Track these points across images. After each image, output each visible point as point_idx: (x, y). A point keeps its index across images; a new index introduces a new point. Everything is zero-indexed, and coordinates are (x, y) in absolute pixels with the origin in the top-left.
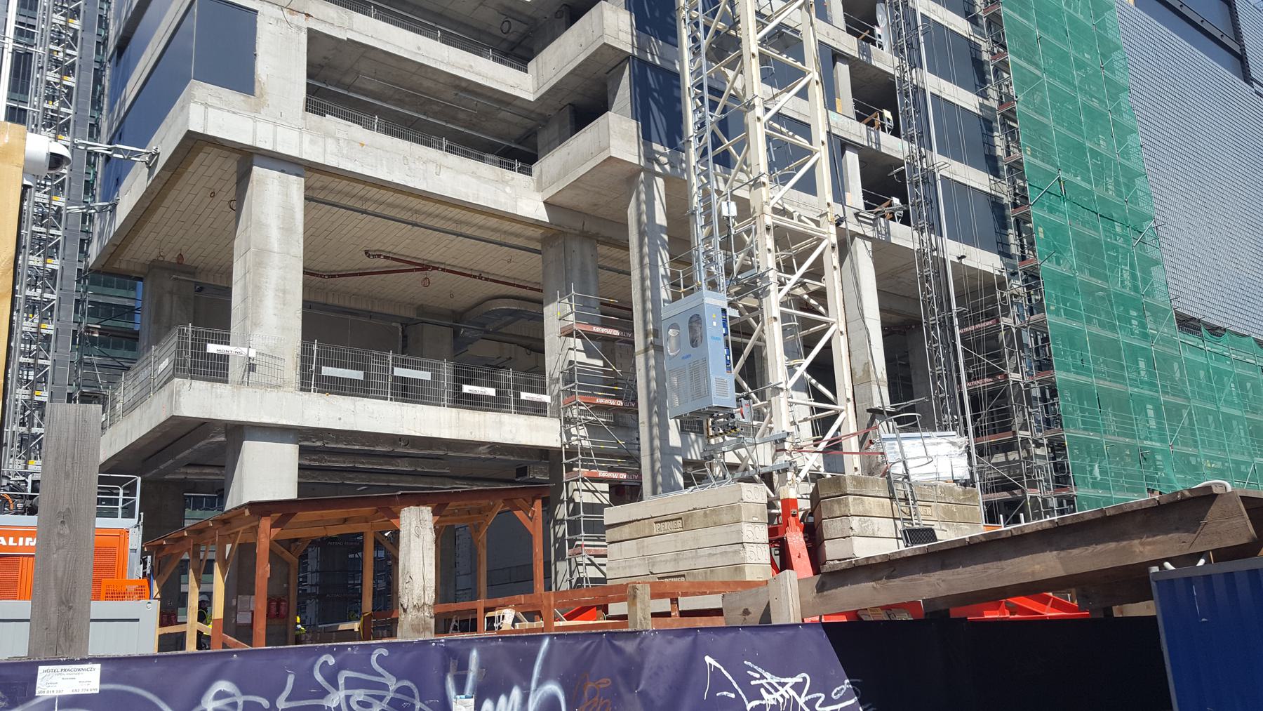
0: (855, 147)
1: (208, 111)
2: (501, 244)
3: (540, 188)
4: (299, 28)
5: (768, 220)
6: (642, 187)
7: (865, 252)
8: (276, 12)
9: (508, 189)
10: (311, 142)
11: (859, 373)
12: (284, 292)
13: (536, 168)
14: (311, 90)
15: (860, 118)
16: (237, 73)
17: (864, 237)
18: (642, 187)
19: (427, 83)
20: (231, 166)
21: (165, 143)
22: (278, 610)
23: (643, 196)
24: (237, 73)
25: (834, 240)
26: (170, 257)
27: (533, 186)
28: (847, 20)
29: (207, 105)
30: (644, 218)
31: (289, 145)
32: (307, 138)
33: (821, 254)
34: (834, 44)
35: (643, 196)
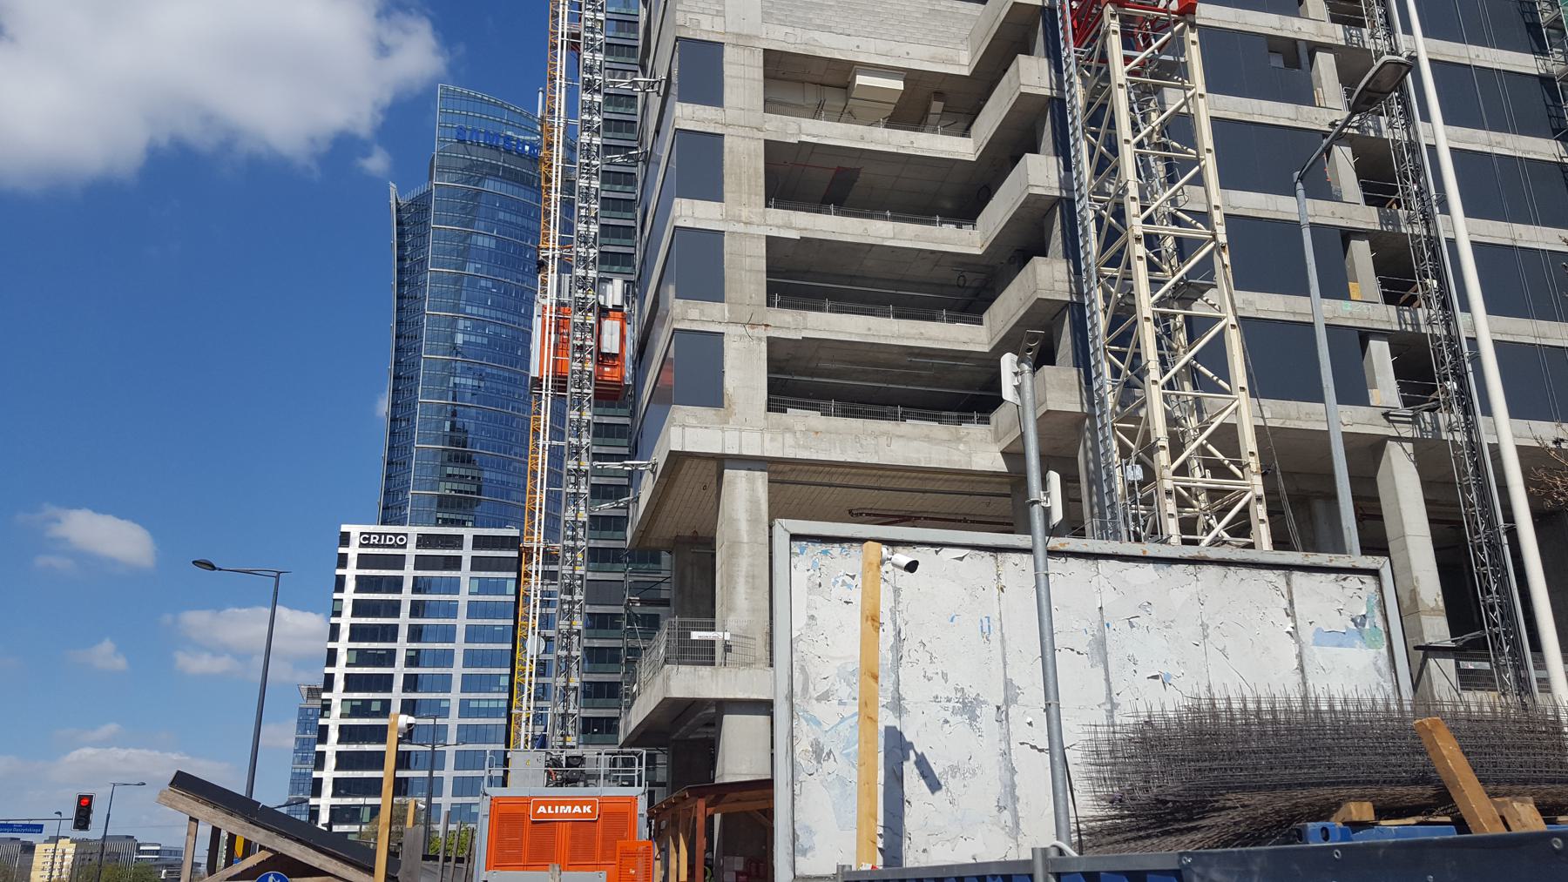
0: (1381, 334)
1: (688, 431)
2: (970, 494)
3: (997, 440)
4: (760, 339)
5: (1168, 484)
6: (1088, 434)
7: (1405, 457)
8: (740, 330)
9: (961, 447)
10: (772, 440)
11: (1406, 602)
12: (753, 577)
13: (994, 417)
14: (773, 387)
15: (1389, 299)
16: (710, 393)
17: (1399, 439)
18: (1088, 434)
19: (882, 356)
20: (713, 465)
21: (660, 457)
22: (757, 868)
23: (1089, 444)
24: (710, 393)
25: (1260, 491)
26: (688, 533)
27: (990, 437)
28: (1365, 187)
29: (684, 426)
30: (1091, 466)
31: (753, 445)
32: (767, 436)
33: (1247, 504)
34: (1343, 223)
35: (1089, 444)
